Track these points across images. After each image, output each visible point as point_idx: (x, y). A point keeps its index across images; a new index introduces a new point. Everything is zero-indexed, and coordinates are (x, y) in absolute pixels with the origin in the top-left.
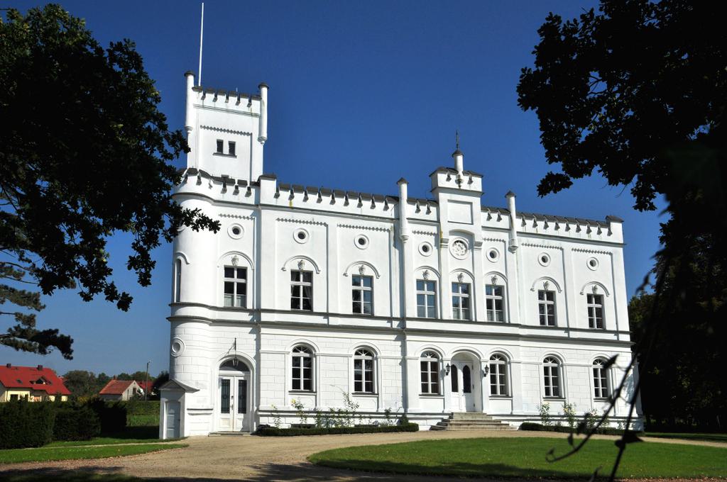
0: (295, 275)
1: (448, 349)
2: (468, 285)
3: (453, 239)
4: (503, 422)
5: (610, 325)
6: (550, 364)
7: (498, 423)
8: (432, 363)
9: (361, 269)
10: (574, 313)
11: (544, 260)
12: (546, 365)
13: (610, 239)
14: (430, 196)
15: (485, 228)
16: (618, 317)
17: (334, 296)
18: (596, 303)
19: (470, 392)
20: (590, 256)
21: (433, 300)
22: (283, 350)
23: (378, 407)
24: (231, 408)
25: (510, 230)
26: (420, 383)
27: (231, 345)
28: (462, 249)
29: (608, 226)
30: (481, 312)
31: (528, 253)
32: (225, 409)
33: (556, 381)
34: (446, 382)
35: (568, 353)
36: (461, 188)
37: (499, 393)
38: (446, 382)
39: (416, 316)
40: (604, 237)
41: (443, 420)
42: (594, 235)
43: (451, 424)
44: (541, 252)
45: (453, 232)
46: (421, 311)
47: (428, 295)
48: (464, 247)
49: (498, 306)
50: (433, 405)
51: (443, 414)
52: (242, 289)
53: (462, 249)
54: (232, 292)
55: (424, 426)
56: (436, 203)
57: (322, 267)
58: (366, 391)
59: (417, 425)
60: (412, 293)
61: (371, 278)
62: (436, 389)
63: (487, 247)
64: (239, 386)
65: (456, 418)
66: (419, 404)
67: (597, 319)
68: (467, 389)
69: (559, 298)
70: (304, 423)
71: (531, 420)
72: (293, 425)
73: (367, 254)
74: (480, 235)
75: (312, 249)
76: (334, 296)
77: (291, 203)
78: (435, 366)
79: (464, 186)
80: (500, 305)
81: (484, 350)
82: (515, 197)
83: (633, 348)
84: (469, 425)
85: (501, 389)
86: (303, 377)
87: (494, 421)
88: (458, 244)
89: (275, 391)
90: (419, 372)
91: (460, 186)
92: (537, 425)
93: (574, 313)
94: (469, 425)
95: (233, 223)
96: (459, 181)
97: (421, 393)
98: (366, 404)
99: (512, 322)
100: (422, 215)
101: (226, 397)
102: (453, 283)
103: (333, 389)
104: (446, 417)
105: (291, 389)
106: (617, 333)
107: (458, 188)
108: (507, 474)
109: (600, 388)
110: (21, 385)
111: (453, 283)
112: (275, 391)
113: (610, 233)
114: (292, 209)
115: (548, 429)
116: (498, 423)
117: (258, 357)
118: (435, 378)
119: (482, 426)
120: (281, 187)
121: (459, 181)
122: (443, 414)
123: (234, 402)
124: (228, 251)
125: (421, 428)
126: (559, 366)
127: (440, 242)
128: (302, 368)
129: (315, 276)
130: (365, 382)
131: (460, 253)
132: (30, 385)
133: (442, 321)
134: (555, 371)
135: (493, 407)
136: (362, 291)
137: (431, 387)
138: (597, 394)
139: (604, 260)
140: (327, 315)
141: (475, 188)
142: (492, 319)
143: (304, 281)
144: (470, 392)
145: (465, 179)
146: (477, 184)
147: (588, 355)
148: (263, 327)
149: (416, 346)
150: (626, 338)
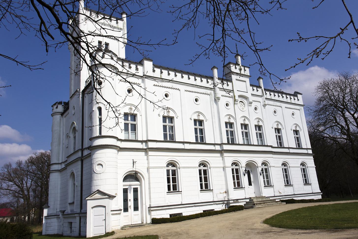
0: (164, 118)
1: (243, 160)
3: (240, 99)
4: (276, 200)
6: (171, 168)
7: (275, 201)
8: (172, 170)
11: (196, 100)
15: (252, 95)
17: (185, 132)
18: (131, 120)
20: (195, 96)
22: (279, 166)
24: (129, 208)
28: (242, 105)
33: (174, 180)
34: (244, 180)
35: (214, 160)
36: (241, 73)
38: (244, 180)
41: (247, 202)
45: (240, 96)
47: (131, 124)
48: (243, 104)
51: (245, 199)
52: (134, 128)
53: (242, 105)
54: (128, 130)
56: (231, 81)
57: (179, 114)
58: (205, 188)
69: (283, 131)
71: (282, 198)
72: (171, 215)
73: (200, 107)
74: (251, 98)
76: (185, 132)
77: (161, 76)
79: (243, 72)
81: (258, 159)
82: (217, 69)
84: (264, 203)
88: (241, 102)
89: (155, 192)
91: (241, 72)
94: (264, 203)
95: (127, 86)
96: (240, 70)
97: (168, 191)
99: (207, 142)
101: (126, 200)
104: (248, 200)
106: (307, 149)
107: (240, 73)
109: (171, 184)
113: (298, 100)
114: (162, 80)
120: (155, 66)
121: (240, 70)
122: (245, 199)
123: (131, 203)
124: (255, 118)
126: (239, 167)
134: (174, 173)
138: (201, 187)
139: (297, 112)
141: (247, 74)
143: (131, 120)
146: (247, 72)
148: (150, 151)
150: (310, 152)
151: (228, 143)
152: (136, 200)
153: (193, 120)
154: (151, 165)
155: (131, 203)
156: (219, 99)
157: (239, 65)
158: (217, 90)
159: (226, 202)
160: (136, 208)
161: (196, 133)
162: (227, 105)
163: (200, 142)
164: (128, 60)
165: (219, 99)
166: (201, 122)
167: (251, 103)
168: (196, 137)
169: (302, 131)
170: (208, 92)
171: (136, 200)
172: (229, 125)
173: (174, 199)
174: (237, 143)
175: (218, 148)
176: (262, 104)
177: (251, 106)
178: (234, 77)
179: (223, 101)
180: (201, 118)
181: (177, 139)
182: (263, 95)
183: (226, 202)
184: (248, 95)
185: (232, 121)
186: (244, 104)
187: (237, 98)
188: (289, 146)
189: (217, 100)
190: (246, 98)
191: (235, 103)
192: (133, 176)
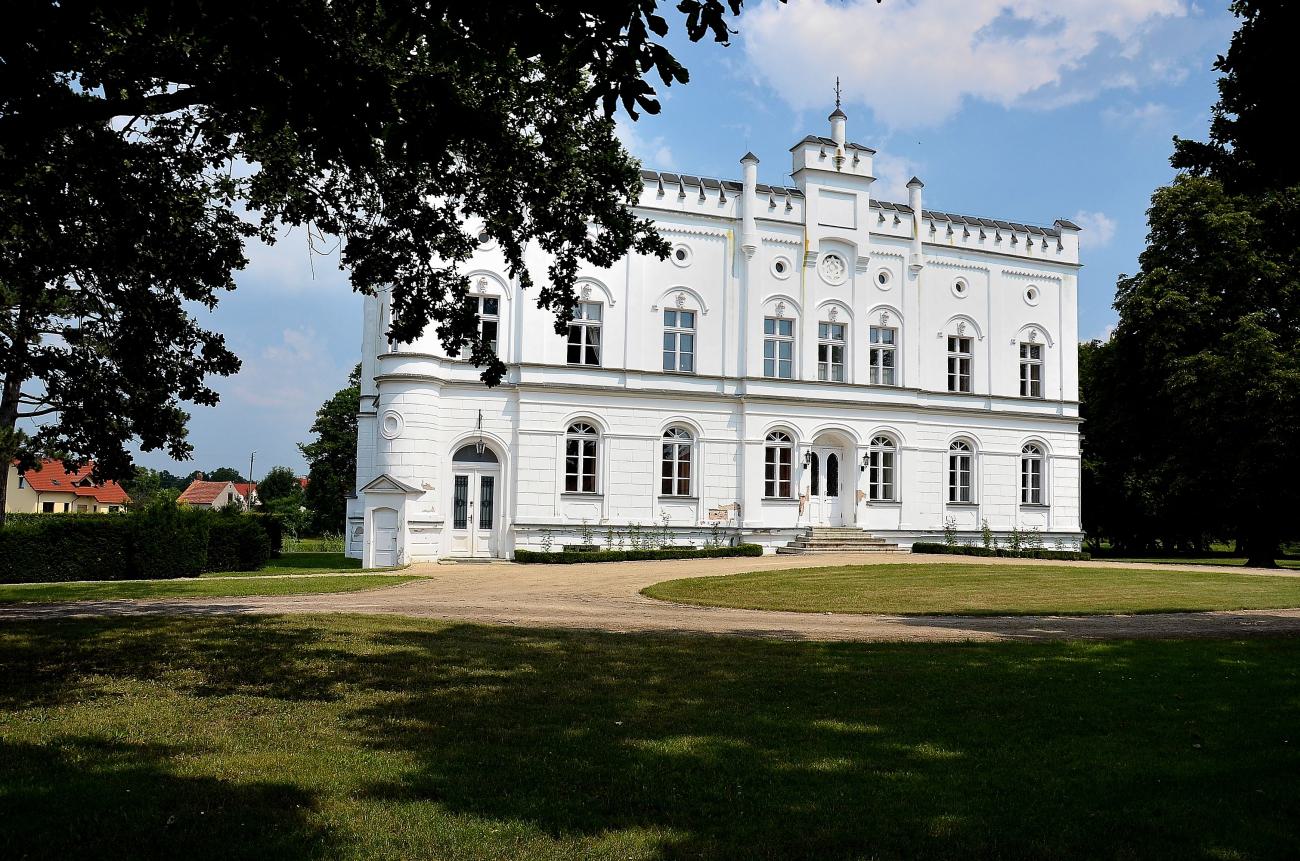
0: (670, 315)
1: (807, 429)
2: (893, 331)
5: (1050, 390)
9: (680, 299)
10: (996, 373)
12: (770, 444)
13: (1062, 257)
14: (791, 184)
16: (1063, 380)
19: (836, 495)
20: (954, 276)
21: (787, 348)
23: (1049, 525)
24: (468, 522)
25: (738, 221)
26: (763, 480)
27: (474, 423)
28: (836, 267)
29: (1056, 235)
30: (858, 367)
31: (938, 279)
32: (460, 523)
34: (802, 481)
35: (711, 424)
36: (841, 171)
37: (675, 492)
39: (660, 369)
40: (1051, 253)
41: (797, 539)
42: (1036, 251)
43: (812, 545)
44: (954, 276)
46: (769, 365)
49: (884, 359)
50: (782, 516)
53: (836, 267)
55: (769, 547)
56: (798, 193)
57: (1055, 338)
59: (761, 547)
60: (757, 337)
61: (600, 305)
62: (785, 490)
63: (875, 267)
64: (483, 485)
65: (817, 535)
66: (761, 514)
67: (1032, 378)
68: (832, 490)
70: (588, 544)
72: (566, 547)
74: (865, 247)
75: (971, 304)
78: (786, 455)
79: (846, 168)
80: (889, 358)
83: (1083, 429)
84: (837, 545)
85: (883, 491)
86: (582, 470)
87: (875, 540)
89: (535, 492)
90: (762, 464)
91: (839, 168)
92: (938, 546)
93: (996, 373)
95: (958, 275)
96: (839, 160)
97: (764, 497)
98: (681, 514)
100: (779, 212)
101: (460, 503)
102: (820, 323)
103: (629, 493)
104: (803, 534)
105: (564, 492)
108: (936, 620)
110: (57, 489)
111: (820, 323)
112: (535, 492)
113: (1060, 248)
115: (956, 551)
116: (881, 544)
117: (515, 445)
118: (785, 472)
119: (858, 548)
121: (839, 160)
123: (474, 511)
124: (667, 288)
125: (766, 551)
127: (807, 258)
128: (676, 462)
129: (700, 319)
130: (676, 477)
131: (833, 274)
132: (71, 489)
133: (854, 386)
135: (874, 519)
136: (831, 347)
137: (779, 486)
140: (623, 372)
142: (876, 380)
144: (836, 495)
145: (848, 156)
147: (1013, 439)
149: (759, 425)
150: (1074, 412)
151: (768, 379)
152: (487, 504)
153: (661, 313)
154: (522, 427)
155: (474, 511)
156: (751, 250)
157: (836, 145)
158: (750, 225)
159: (733, 532)
160: (486, 523)
161: (951, 368)
162: (780, 267)
163: (678, 370)
164: (1225, 194)
165: (751, 250)
166: (965, 344)
167: (864, 261)
168: (951, 380)
169: (1056, 347)
170: (723, 230)
171: (487, 504)
172: (780, 326)
173: (582, 511)
174: (850, 382)
175: (730, 389)
176: (907, 263)
177: (866, 269)
178: (812, 188)
179: (764, 258)
180: (690, 304)
181: (701, 368)
182: (914, 236)
183: (733, 532)
184: (861, 239)
185: (789, 312)
186: (842, 264)
187: (813, 247)
188: (723, 372)
189: (743, 253)
190: (852, 246)
191: (805, 262)
192: (473, 452)
